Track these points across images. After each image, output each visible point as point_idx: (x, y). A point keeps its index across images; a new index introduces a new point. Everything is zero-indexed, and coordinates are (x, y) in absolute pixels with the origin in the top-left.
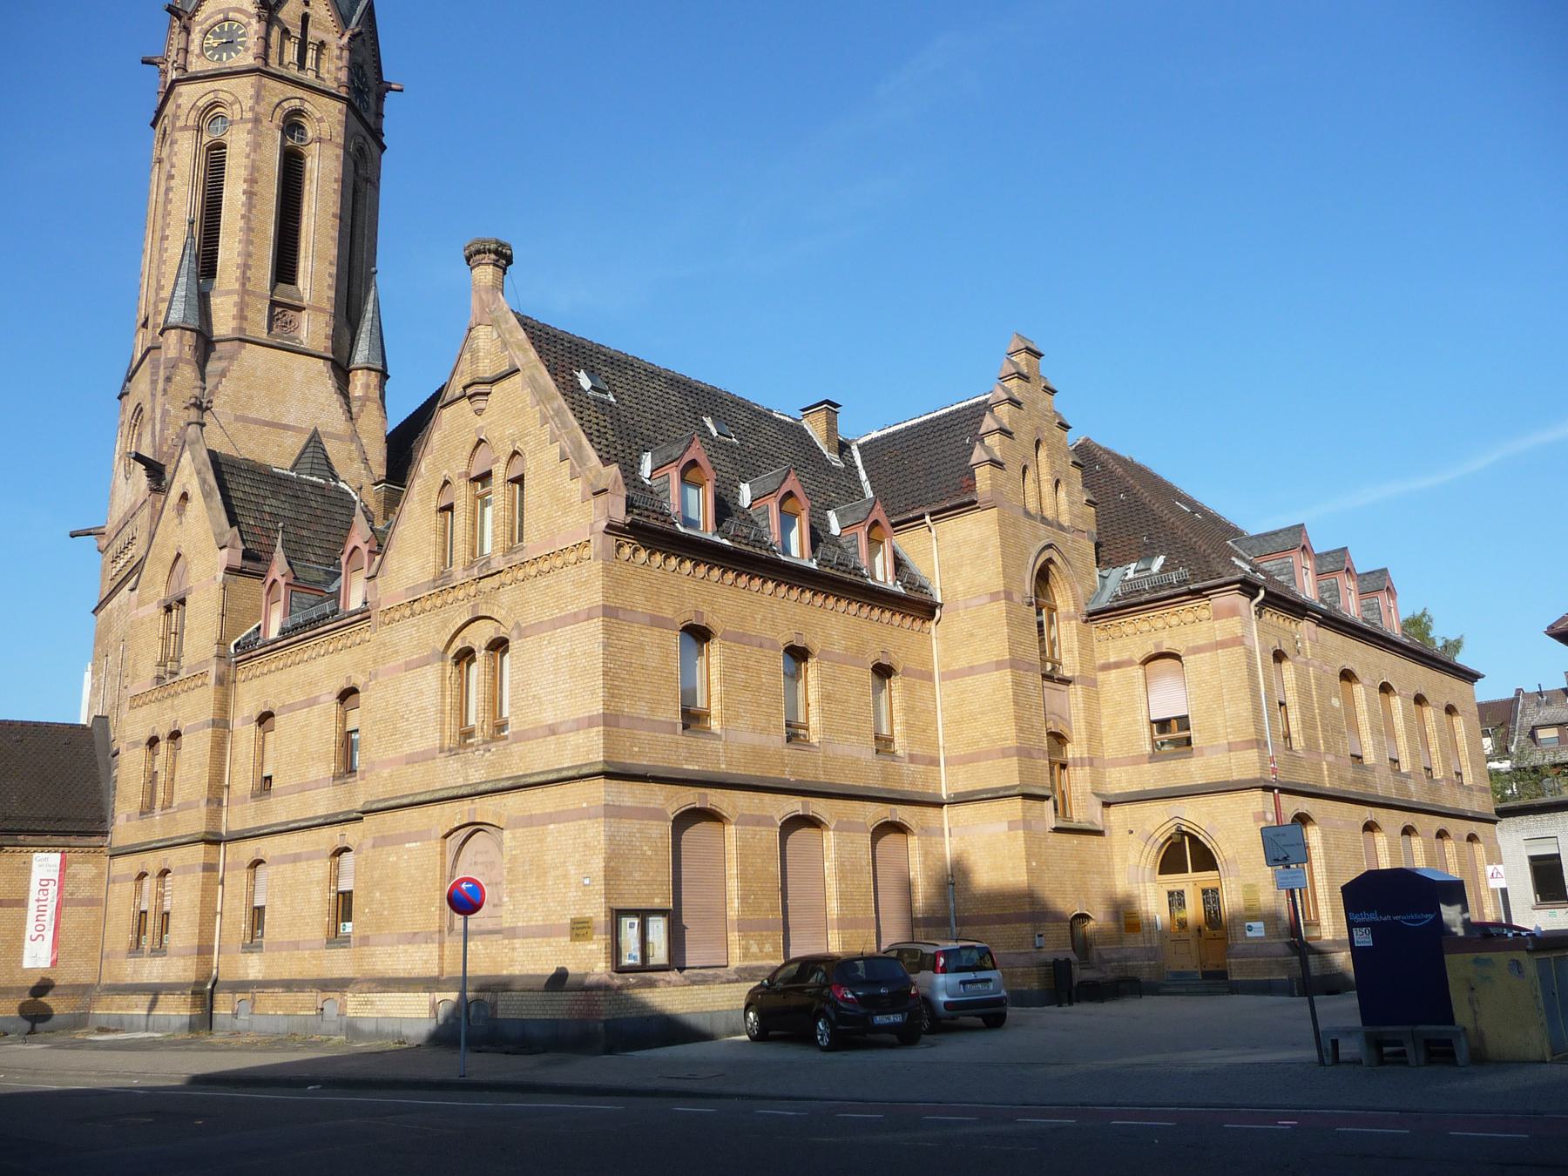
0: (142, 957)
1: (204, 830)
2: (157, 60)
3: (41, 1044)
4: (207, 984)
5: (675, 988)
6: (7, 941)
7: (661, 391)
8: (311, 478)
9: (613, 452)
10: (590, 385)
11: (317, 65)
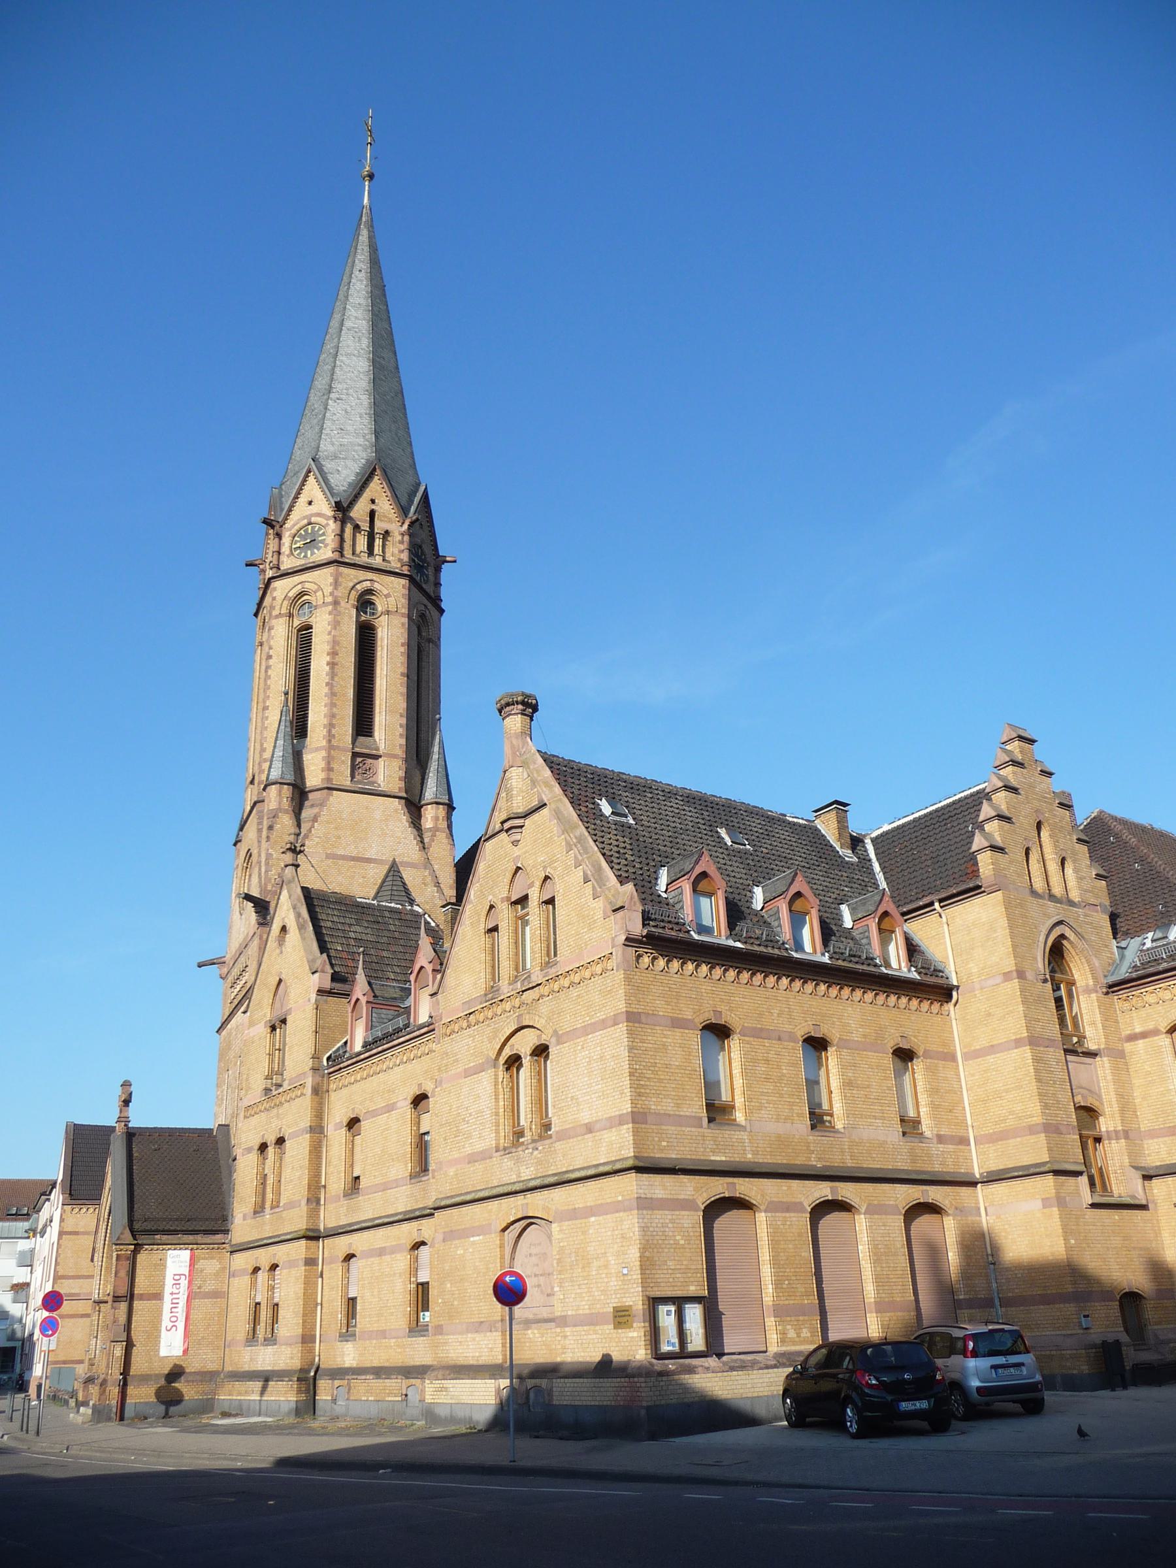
0: (257, 1345)
1: (305, 1227)
2: (257, 562)
3: (172, 1427)
4: (310, 1372)
5: (714, 1375)
6: (147, 1332)
7: (678, 808)
8: (390, 905)
9: (632, 870)
10: (611, 810)
11: (383, 552)
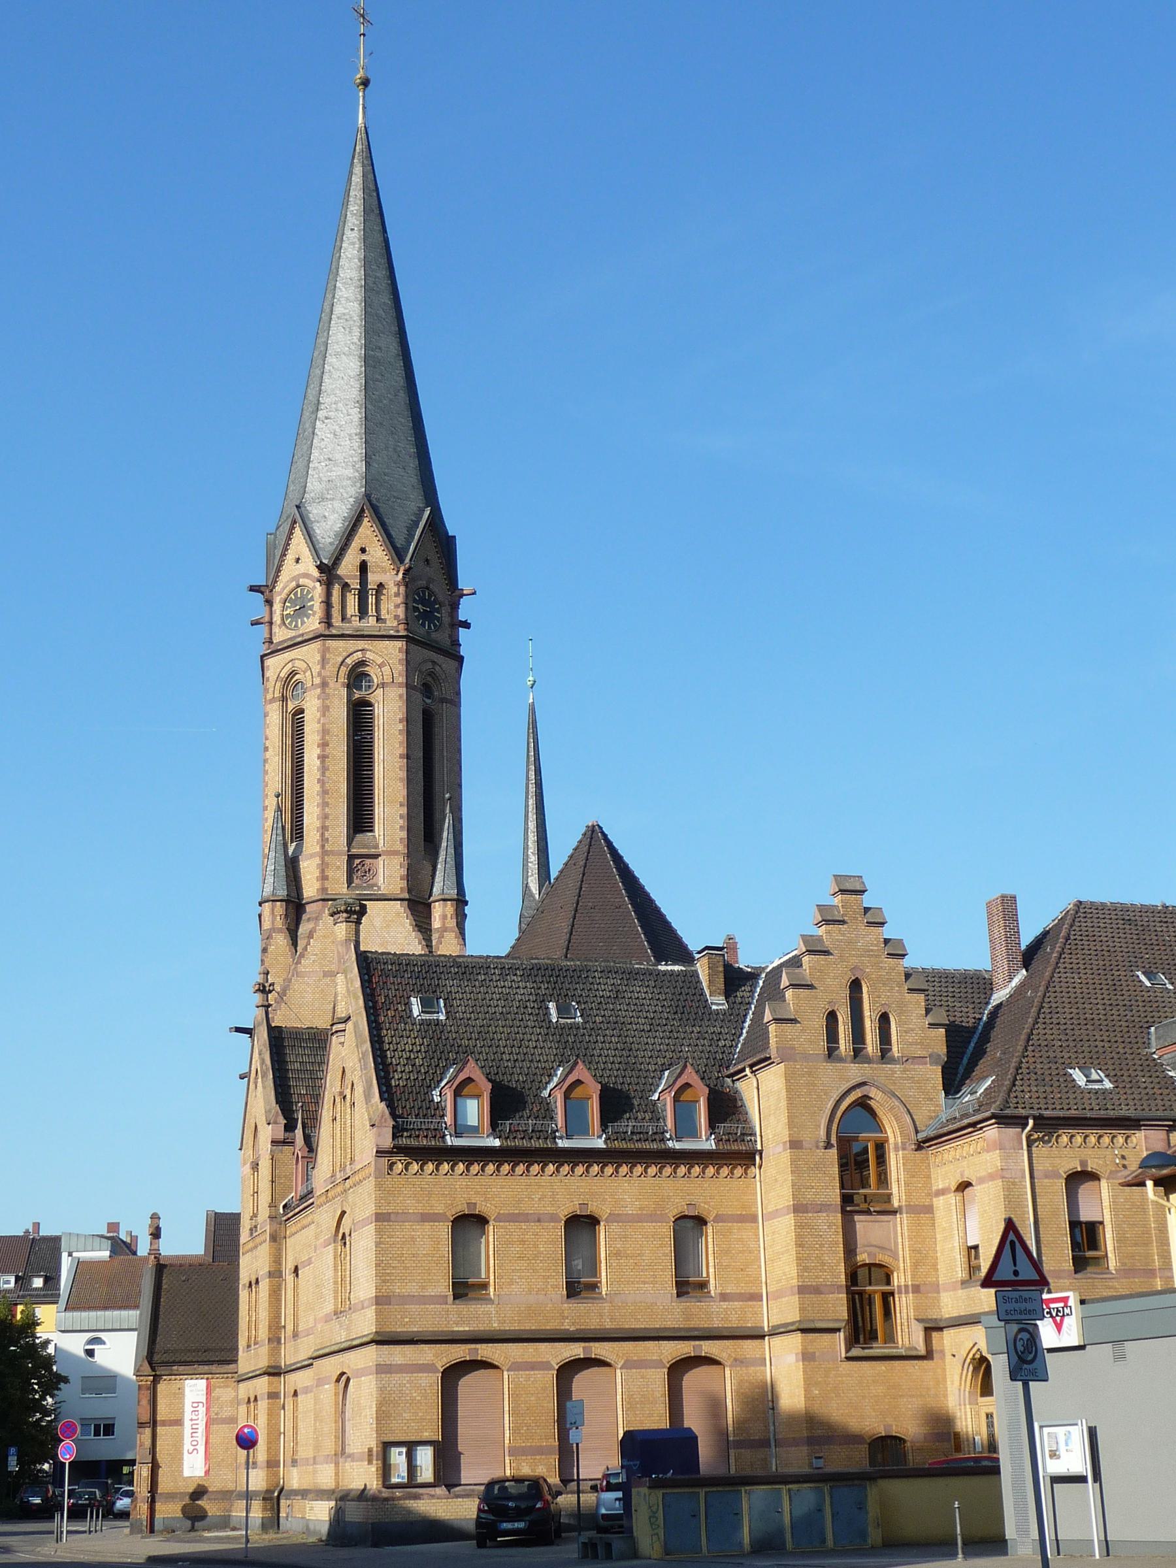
4: (274, 1492)
5: (439, 1501)
6: (170, 1454)
